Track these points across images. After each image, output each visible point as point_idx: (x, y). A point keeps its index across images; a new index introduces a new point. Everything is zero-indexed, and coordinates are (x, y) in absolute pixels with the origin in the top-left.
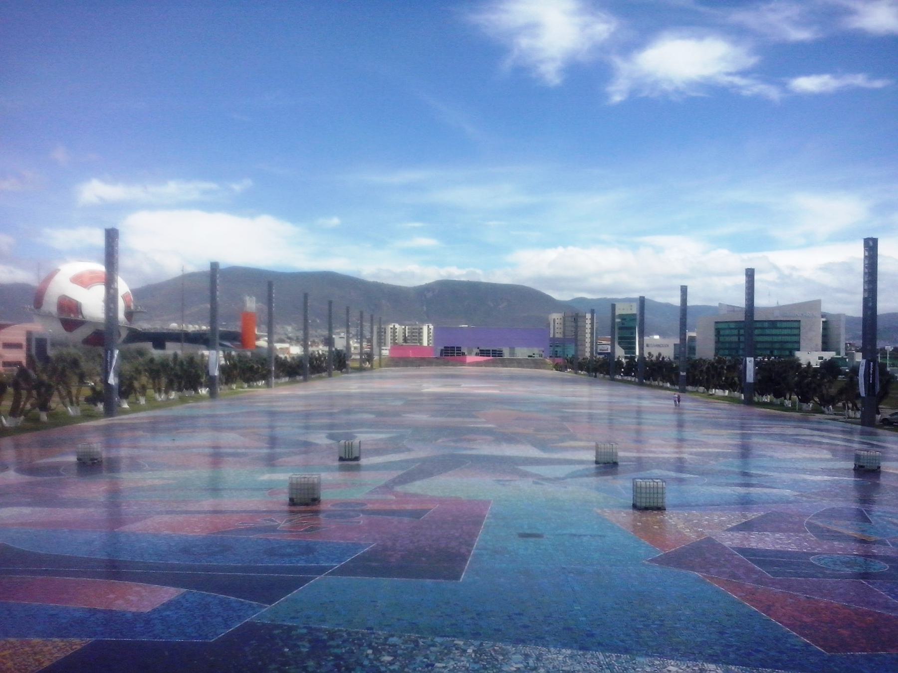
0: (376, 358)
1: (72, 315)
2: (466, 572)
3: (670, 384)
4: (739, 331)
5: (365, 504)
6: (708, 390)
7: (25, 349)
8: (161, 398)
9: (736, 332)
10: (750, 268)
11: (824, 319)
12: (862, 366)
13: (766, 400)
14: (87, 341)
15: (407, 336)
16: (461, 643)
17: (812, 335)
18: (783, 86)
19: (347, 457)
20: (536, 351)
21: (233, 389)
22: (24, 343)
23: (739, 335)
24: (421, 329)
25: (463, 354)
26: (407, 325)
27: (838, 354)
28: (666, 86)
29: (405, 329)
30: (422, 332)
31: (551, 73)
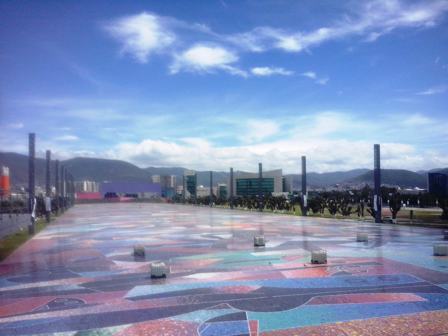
11: (283, 178)
12: (375, 198)
18: (249, 72)
20: (155, 194)
23: (247, 185)
24: (83, 183)
25: (117, 196)
27: (290, 193)
28: (197, 67)
30: (83, 185)
31: (143, 57)
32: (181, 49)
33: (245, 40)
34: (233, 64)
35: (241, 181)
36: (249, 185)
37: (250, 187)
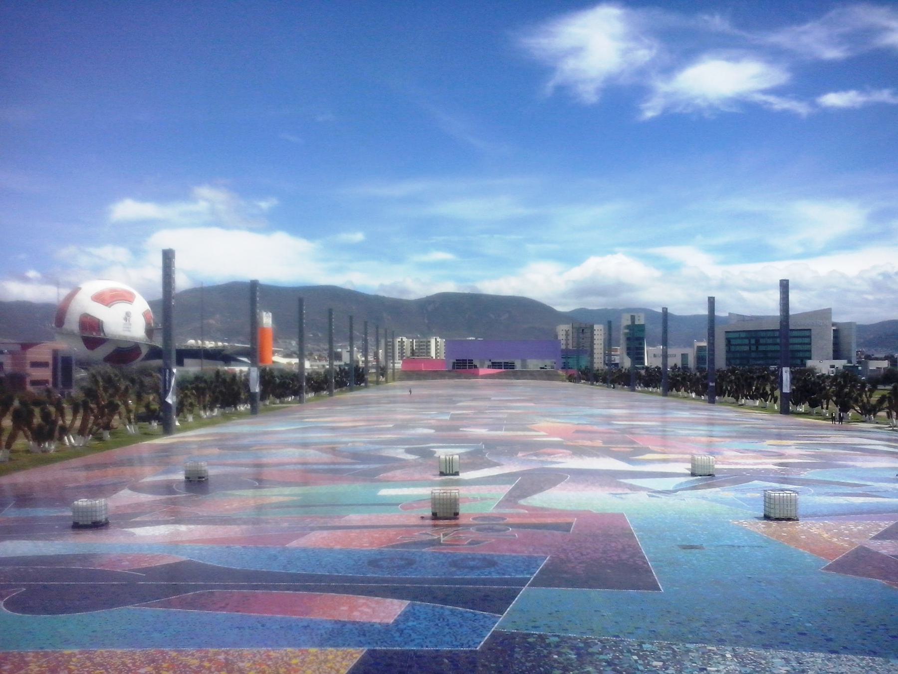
0: (390, 371)
1: (94, 334)
2: (238, 592)
3: (696, 394)
4: (750, 341)
5: (503, 519)
6: (737, 401)
7: (51, 367)
8: (206, 415)
9: (747, 341)
10: (784, 279)
11: (834, 328)
13: (801, 410)
14: (109, 359)
15: (414, 349)
16: (714, 648)
17: (823, 343)
19: (451, 472)
20: (548, 362)
21: (267, 405)
22: (51, 362)
23: (750, 344)
24: (430, 342)
25: (475, 367)
26: (415, 339)
27: (850, 362)
29: (412, 342)
31: (589, 95)
32: (669, 71)
33: (805, 39)
34: (778, 91)
35: (737, 335)
36: (753, 345)
37: (757, 347)
